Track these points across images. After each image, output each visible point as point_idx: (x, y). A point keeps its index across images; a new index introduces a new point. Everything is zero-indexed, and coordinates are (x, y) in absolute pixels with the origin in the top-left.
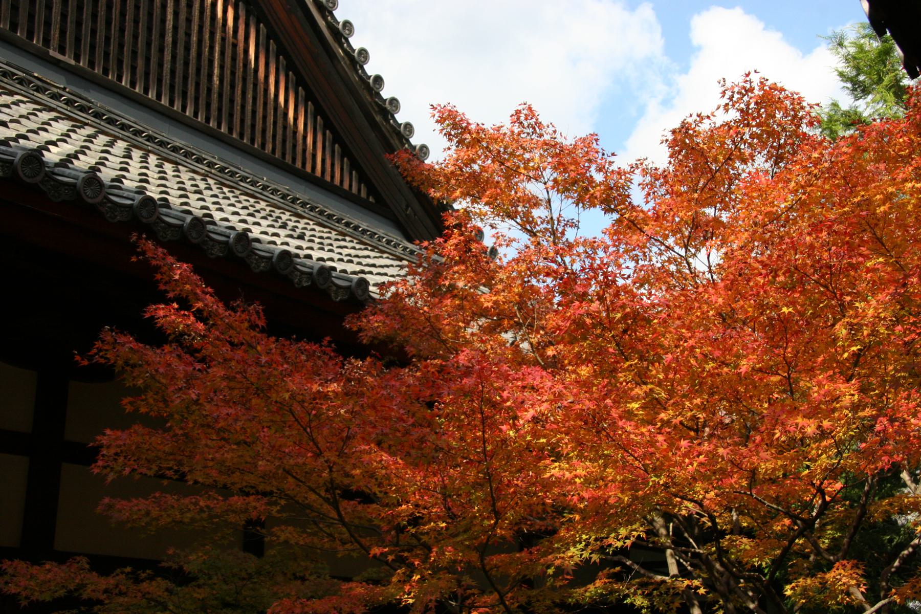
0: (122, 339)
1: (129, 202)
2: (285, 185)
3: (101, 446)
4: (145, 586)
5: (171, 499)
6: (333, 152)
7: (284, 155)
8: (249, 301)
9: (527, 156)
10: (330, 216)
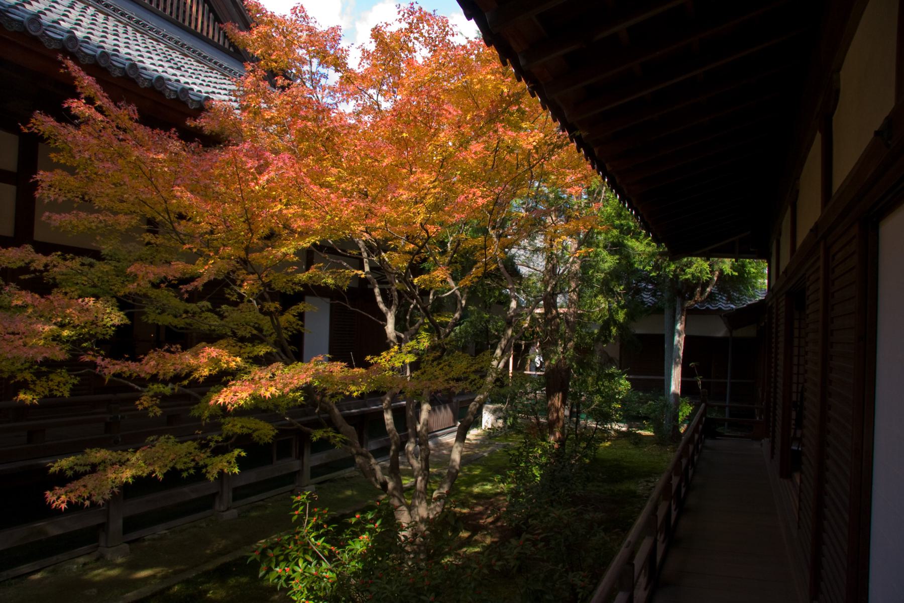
0: (47, 119)
1: (60, 37)
2: (177, 35)
3: (37, 181)
4: (67, 263)
5: (83, 215)
6: (209, 18)
7: (177, 16)
8: (129, 103)
9: (299, 34)
10: (205, 57)
